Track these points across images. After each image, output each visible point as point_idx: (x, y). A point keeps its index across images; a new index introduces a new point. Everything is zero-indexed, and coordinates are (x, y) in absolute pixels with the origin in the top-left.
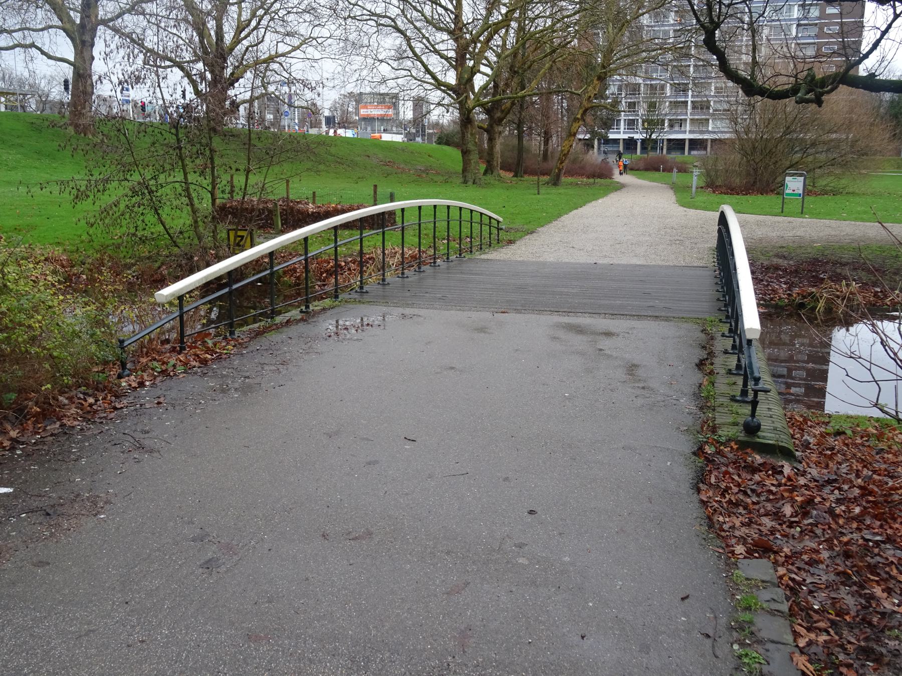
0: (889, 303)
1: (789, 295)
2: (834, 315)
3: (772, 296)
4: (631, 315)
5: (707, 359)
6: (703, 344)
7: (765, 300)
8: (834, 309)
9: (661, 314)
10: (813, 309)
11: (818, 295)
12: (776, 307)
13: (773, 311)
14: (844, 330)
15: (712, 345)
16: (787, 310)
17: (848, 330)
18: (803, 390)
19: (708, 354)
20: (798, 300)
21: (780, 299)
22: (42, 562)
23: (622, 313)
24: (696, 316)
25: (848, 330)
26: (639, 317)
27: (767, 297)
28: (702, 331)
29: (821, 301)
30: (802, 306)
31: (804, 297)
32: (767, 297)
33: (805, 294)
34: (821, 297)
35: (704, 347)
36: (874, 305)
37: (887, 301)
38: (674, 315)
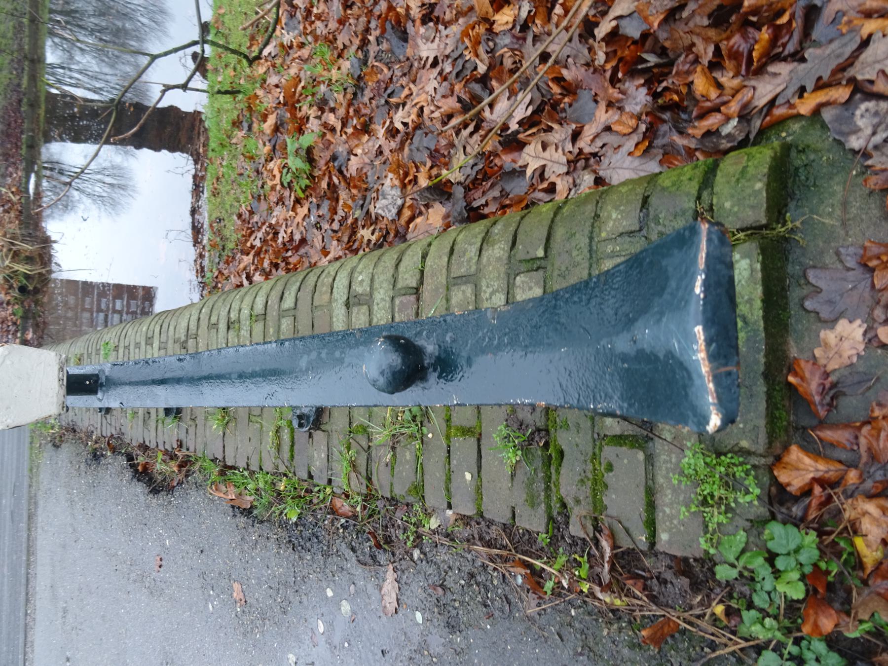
0: (18, 197)
1: (8, 303)
2: (35, 255)
3: (10, 324)
4: (28, 566)
5: (130, 458)
6: (86, 455)
7: (17, 331)
8: (27, 254)
9: (25, 507)
10: (27, 277)
11: (7, 272)
12: (25, 318)
13: (31, 322)
14: (55, 245)
15: (89, 435)
16: (30, 306)
17: (55, 242)
18: (132, 302)
19: (114, 450)
20: (16, 293)
21: (14, 314)
22: (143, 474)
23: (24, 581)
24: (27, 445)
25: (55, 242)
26: (30, 551)
27: (12, 328)
28: (56, 446)
29: (16, 268)
30: (23, 289)
31: (11, 287)
32: (12, 328)
33: (6, 286)
34: (11, 268)
35: (96, 456)
36: (20, 212)
37: (15, 199)
38: (26, 484)
